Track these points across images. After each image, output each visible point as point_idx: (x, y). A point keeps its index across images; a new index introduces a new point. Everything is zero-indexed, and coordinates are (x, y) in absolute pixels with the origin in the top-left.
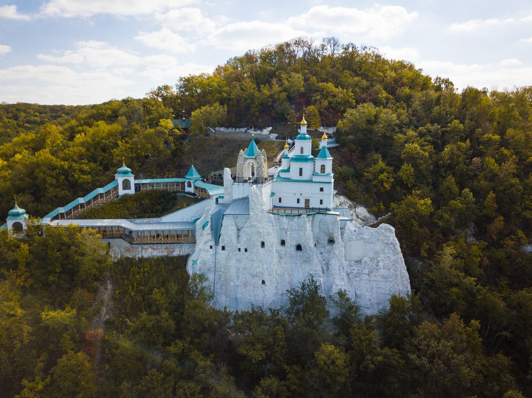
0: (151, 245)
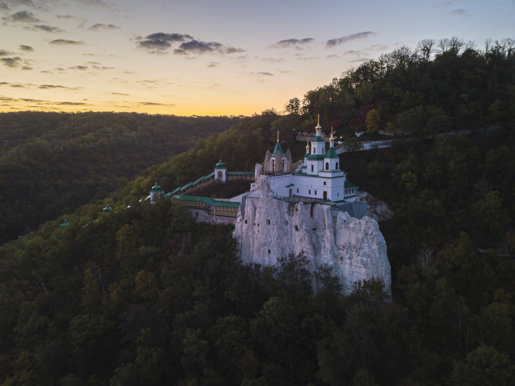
0: (220, 217)
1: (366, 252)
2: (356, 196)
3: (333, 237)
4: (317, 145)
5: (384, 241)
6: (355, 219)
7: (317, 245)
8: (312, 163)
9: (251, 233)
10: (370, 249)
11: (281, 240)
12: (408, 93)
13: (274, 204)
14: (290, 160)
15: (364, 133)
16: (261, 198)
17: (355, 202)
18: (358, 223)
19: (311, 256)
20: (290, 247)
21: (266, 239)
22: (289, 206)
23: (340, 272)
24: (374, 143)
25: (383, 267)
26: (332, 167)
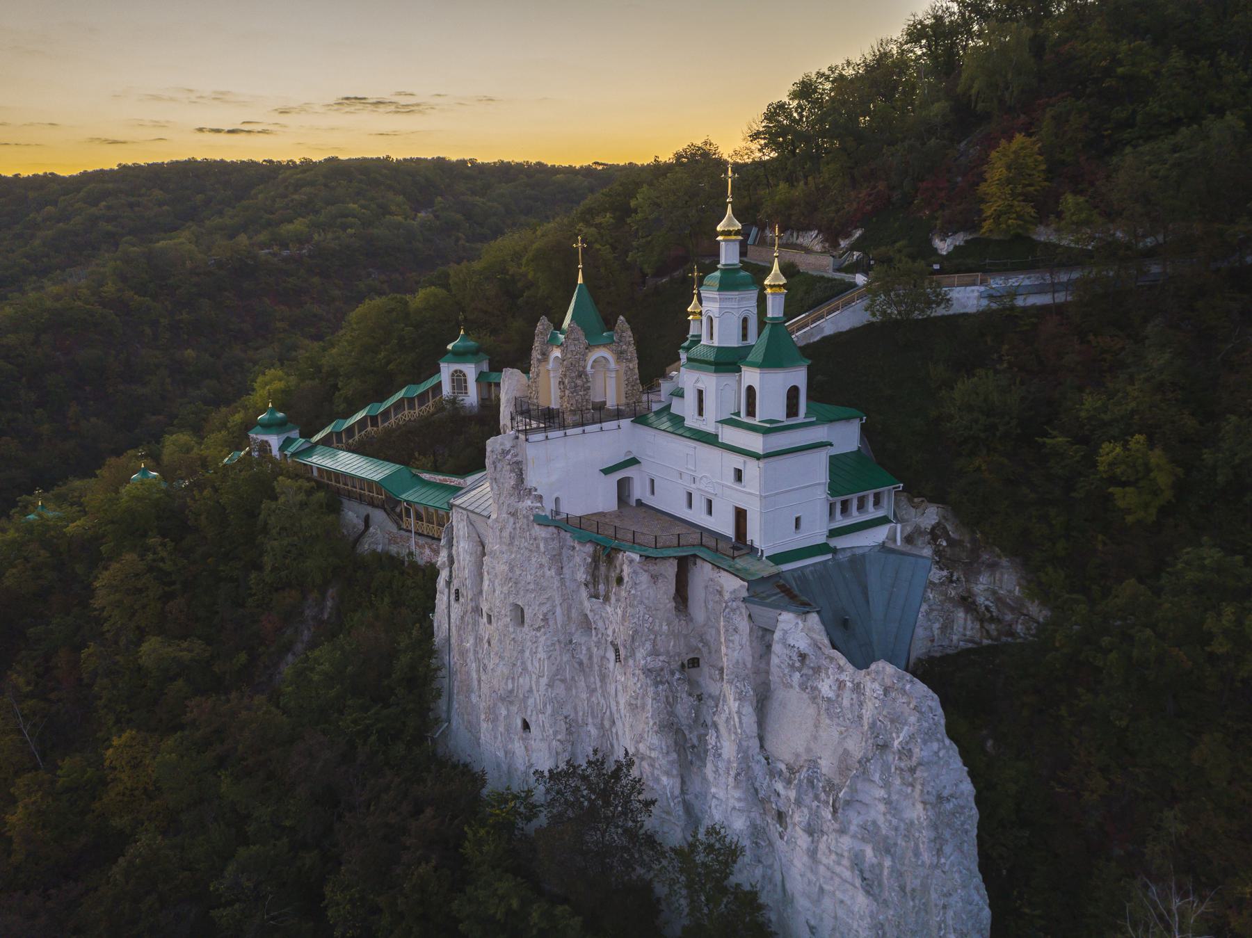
0: (429, 541)
1: (874, 822)
2: (889, 521)
3: (750, 719)
4: (717, 305)
5: (967, 787)
6: (843, 661)
7: (696, 733)
8: (697, 381)
9: (472, 641)
10: (894, 816)
11: (568, 689)
12: (1176, 60)
13: (538, 547)
14: (630, 361)
15: (970, 237)
16: (494, 516)
17: (883, 547)
18: (849, 684)
19: (664, 780)
20: (599, 721)
21: (513, 678)
22: (596, 560)
23: (776, 866)
24: (997, 283)
25: (950, 913)
26: (771, 406)
